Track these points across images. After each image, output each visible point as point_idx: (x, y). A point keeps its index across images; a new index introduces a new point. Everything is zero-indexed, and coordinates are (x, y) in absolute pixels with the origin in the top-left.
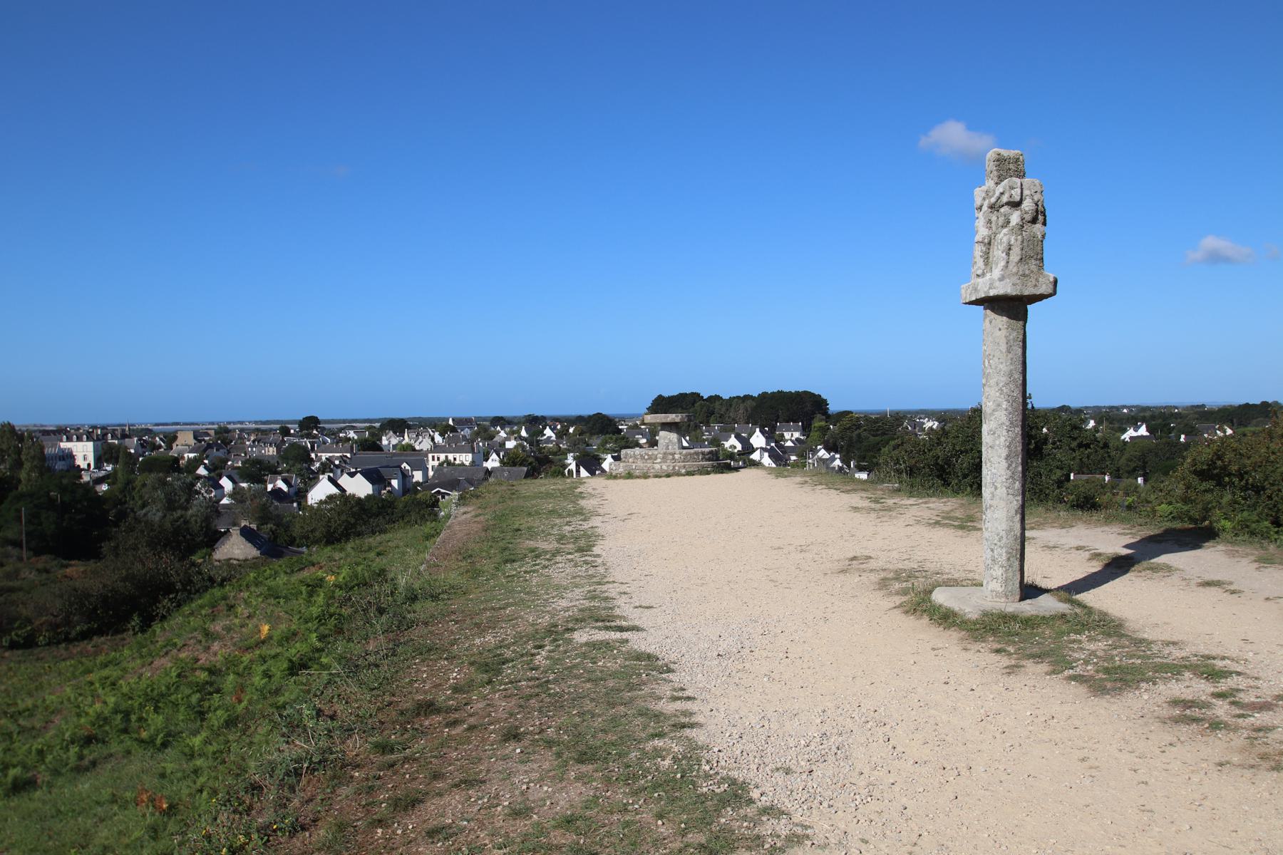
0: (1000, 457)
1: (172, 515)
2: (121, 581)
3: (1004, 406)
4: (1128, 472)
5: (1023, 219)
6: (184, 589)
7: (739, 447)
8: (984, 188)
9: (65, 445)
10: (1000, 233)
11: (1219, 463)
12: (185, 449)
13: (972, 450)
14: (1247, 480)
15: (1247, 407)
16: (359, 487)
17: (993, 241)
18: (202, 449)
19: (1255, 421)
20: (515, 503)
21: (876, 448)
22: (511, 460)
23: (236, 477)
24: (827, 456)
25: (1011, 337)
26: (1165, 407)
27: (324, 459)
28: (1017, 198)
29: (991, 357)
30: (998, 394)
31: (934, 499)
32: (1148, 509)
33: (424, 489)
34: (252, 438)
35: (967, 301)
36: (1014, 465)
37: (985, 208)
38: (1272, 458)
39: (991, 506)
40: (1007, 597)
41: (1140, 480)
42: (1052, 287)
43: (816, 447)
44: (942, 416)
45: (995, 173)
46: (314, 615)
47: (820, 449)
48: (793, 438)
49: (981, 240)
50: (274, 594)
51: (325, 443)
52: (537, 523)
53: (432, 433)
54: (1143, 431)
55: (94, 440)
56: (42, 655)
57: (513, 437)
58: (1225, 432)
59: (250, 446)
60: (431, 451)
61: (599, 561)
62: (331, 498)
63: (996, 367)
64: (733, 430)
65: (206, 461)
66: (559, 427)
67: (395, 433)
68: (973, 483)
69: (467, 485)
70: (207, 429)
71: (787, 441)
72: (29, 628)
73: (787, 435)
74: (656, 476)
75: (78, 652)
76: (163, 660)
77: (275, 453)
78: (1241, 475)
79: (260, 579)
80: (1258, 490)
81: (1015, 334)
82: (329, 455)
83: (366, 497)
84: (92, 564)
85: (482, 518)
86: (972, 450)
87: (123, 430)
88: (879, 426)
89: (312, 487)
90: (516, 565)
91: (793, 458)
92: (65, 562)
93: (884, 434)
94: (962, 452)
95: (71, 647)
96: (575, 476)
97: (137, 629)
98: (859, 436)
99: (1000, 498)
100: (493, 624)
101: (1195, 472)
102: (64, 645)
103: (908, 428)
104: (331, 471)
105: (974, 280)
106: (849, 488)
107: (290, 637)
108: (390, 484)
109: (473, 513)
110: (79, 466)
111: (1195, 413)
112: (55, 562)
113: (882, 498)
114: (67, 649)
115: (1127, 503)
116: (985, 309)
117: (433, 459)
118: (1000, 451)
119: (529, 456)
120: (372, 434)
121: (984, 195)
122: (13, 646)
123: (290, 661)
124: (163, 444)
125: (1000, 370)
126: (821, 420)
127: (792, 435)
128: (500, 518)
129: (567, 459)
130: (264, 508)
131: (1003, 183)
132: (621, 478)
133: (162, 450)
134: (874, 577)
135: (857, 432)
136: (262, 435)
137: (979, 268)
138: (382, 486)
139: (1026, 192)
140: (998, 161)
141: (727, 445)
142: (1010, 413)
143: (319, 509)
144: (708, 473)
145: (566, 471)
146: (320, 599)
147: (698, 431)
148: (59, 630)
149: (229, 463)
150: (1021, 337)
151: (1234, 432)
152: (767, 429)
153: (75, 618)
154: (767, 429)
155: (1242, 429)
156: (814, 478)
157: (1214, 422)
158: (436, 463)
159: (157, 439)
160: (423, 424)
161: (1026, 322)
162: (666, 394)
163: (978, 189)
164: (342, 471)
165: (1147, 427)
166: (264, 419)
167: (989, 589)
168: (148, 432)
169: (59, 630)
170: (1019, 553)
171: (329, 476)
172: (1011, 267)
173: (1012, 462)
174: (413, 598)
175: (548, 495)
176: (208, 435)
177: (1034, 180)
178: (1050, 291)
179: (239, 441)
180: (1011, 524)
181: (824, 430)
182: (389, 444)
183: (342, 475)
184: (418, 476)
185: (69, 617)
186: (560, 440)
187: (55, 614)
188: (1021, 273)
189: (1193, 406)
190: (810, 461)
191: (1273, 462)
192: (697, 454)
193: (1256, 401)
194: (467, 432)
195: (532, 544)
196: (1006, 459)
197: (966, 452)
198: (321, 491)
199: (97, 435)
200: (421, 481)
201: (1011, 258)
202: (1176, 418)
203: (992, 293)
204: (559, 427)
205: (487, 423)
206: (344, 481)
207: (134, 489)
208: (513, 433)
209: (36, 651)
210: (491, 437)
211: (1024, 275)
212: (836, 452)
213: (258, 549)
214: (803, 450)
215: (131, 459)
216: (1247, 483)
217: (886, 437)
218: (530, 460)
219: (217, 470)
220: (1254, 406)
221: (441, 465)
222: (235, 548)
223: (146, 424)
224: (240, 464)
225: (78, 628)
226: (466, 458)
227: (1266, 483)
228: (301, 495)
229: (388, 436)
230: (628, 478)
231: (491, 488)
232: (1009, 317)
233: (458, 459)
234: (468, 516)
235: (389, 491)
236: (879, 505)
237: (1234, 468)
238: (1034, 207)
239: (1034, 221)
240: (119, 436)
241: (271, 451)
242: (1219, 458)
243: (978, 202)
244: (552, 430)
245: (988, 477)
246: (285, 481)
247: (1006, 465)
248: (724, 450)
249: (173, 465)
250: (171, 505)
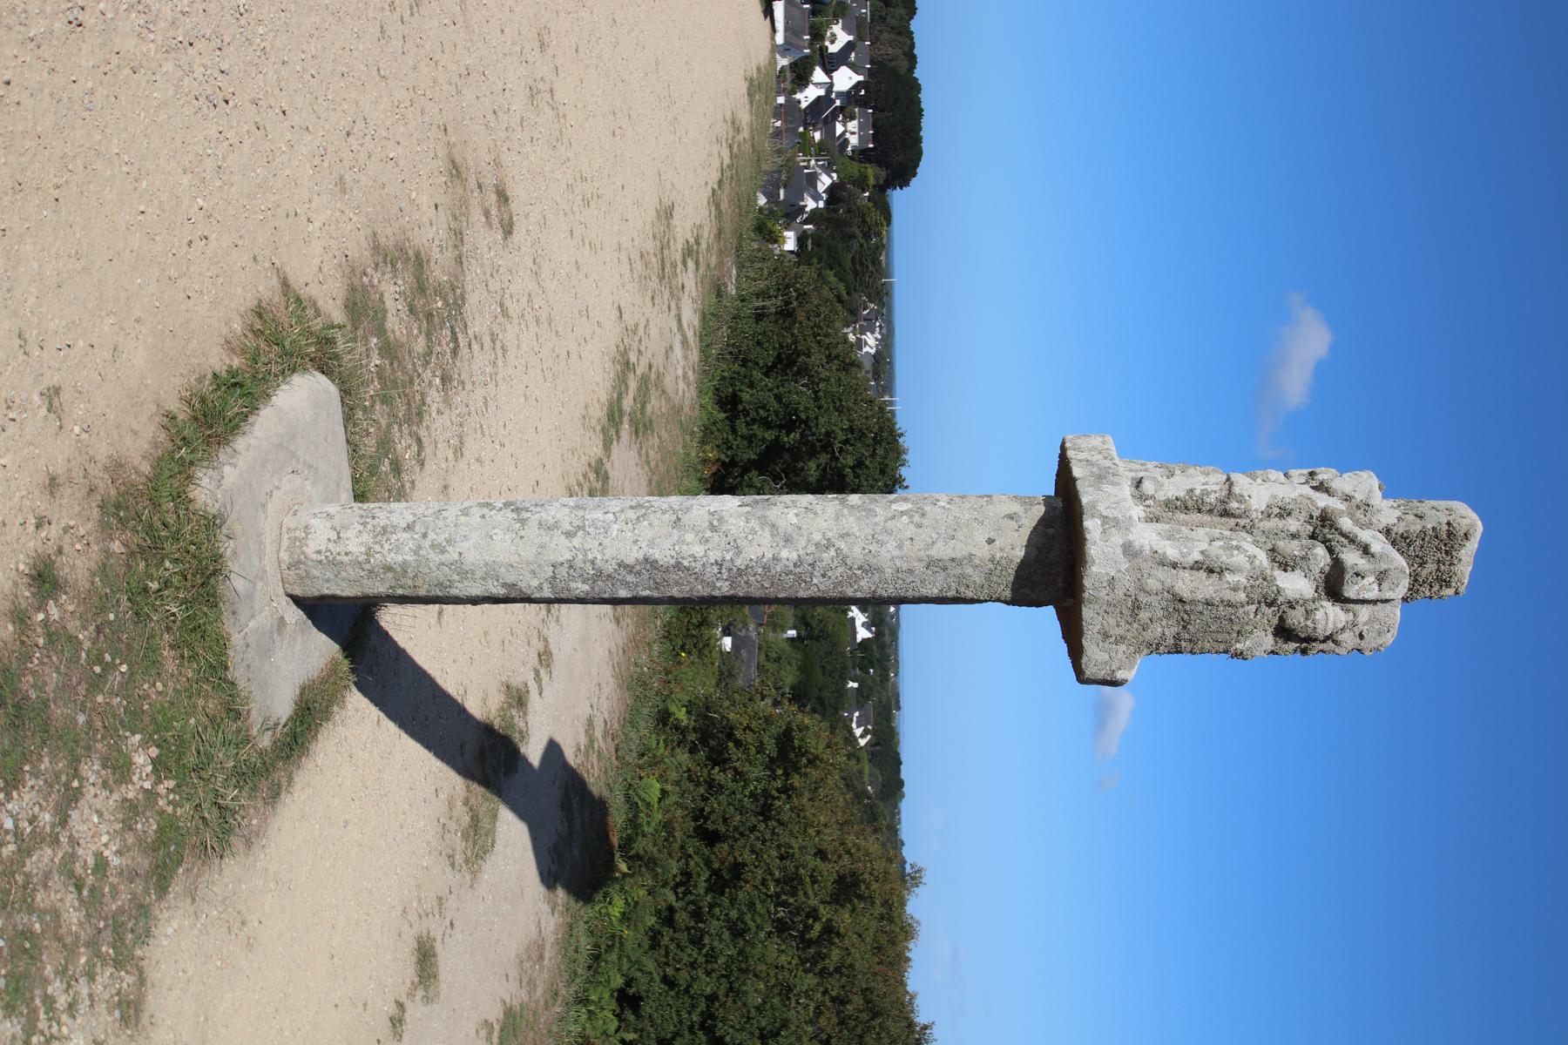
0: (652, 544)
3: (784, 554)
4: (803, 617)
5: (1291, 605)
7: (833, 48)
8: (1377, 499)
10: (1256, 543)
11: (804, 760)
13: (820, 407)
14: (778, 798)
15: (898, 762)
17: (1232, 521)
19: (878, 772)
21: (834, 263)
24: (821, 188)
25: (969, 571)
26: (897, 661)
28: (1350, 591)
29: (917, 518)
30: (817, 537)
31: (695, 356)
32: (661, 750)
35: (1070, 454)
36: (630, 578)
37: (1322, 501)
38: (811, 831)
39: (523, 522)
40: (295, 565)
41: (792, 633)
42: (1101, 675)
43: (835, 171)
44: (883, 360)
45: (1417, 527)
47: (831, 178)
48: (848, 135)
49: (1236, 490)
54: (863, 634)
58: (862, 736)
63: (889, 532)
64: (860, 38)
68: (769, 410)
71: (845, 125)
73: (853, 125)
78: (786, 790)
80: (765, 812)
81: (978, 578)
86: (820, 407)
88: (867, 267)
93: (856, 274)
94: (816, 392)
98: (853, 236)
99: (542, 546)
101: (788, 731)
103: (865, 309)
105: (1126, 471)
106: (724, 206)
111: (889, 700)
113: (697, 264)
115: (673, 708)
116: (1047, 500)
118: (667, 544)
121: (1359, 497)
125: (881, 543)
126: (876, 178)
127: (853, 133)
131: (1395, 554)
134: (430, 235)
135: (858, 233)
137: (1159, 486)
139: (1364, 612)
140: (1450, 534)
141: (837, 29)
142: (766, 568)
150: (969, 594)
151: (861, 748)
152: (863, 92)
154: (863, 92)
155: (865, 757)
156: (748, 145)
157: (875, 724)
161: (1007, 603)
163: (1375, 482)
165: (868, 639)
167: (313, 522)
170: (407, 592)
172: (1161, 573)
173: (639, 573)
177: (1394, 632)
178: (1089, 672)
180: (479, 574)
181: (861, 183)
188: (1143, 598)
189: (897, 695)
190: (813, 162)
191: (805, 832)
193: (905, 773)
196: (646, 560)
197: (817, 399)
201: (1186, 574)
202: (881, 675)
203: (1091, 525)
211: (1136, 607)
212: (827, 202)
214: (832, 151)
216: (774, 798)
217: (851, 277)
220: (898, 771)
227: (775, 824)
232: (1023, 565)
236: (678, 257)
237: (796, 781)
238: (1321, 632)
239: (1283, 632)
242: (811, 762)
243: (1344, 483)
245: (599, 515)
247: (630, 561)
248: (828, 25)
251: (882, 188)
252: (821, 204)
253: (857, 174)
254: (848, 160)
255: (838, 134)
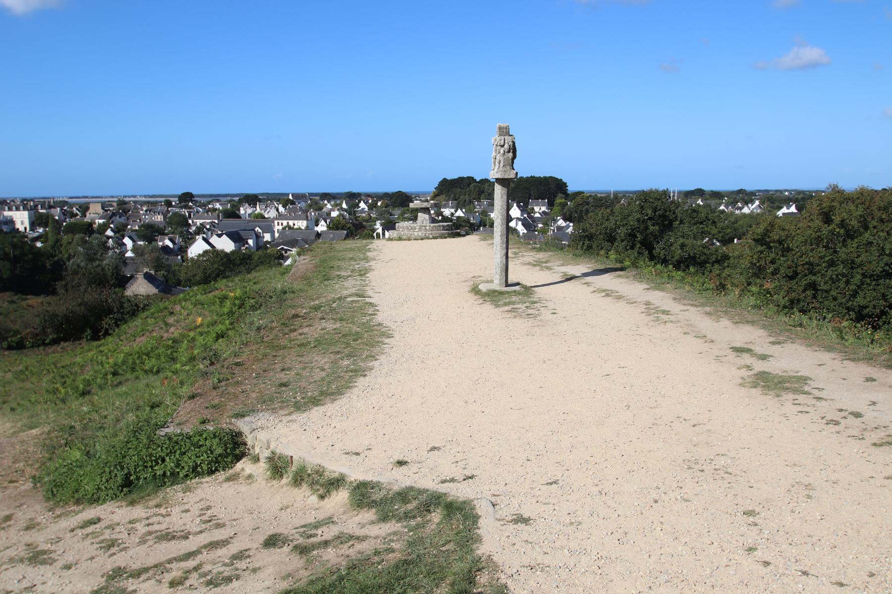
1: (92, 264)
2: (77, 306)
6: (118, 312)
9: (7, 213)
12: (95, 216)
13: (627, 224)
16: (225, 245)
18: (108, 216)
20: (332, 254)
22: (335, 226)
23: (135, 238)
27: (198, 224)
33: (272, 246)
34: (144, 209)
46: (226, 313)
47: (559, 219)
48: (541, 211)
50: (197, 304)
51: (198, 212)
52: (343, 264)
53: (277, 205)
54: (793, 209)
55: (28, 210)
56: (28, 354)
57: (336, 209)
59: (143, 214)
60: (277, 219)
61: (368, 279)
62: (206, 252)
65: (112, 226)
66: (370, 201)
67: (250, 205)
69: (303, 243)
70: (109, 201)
71: (536, 212)
72: (19, 336)
73: (536, 209)
74: (415, 239)
75: (52, 352)
76: (142, 338)
77: (162, 220)
79: (188, 297)
82: (202, 221)
83: (231, 252)
84: (49, 299)
85: (314, 261)
86: (627, 224)
87: (49, 202)
89: (191, 244)
90: (330, 281)
91: (540, 225)
92: (24, 297)
95: (47, 349)
96: (381, 237)
97: (89, 338)
100: (318, 298)
101: (754, 240)
102: (42, 347)
104: (204, 233)
107: (214, 324)
108: (247, 243)
109: (309, 259)
110: (18, 229)
112: (17, 297)
114: (44, 350)
117: (278, 225)
119: (349, 223)
120: (232, 206)
122: (10, 348)
123: (217, 333)
124: (78, 213)
126: (562, 198)
128: (324, 261)
129: (375, 225)
130: (158, 259)
132: (395, 240)
133: (78, 217)
136: (152, 206)
138: (242, 244)
139: (506, 142)
143: (198, 260)
144: (446, 238)
145: (375, 234)
146: (228, 303)
147: (472, 205)
148: (39, 338)
149: (129, 227)
152: (522, 204)
153: (49, 330)
154: (522, 204)
158: (280, 227)
159: (74, 209)
160: (270, 198)
162: (449, 178)
164: (212, 233)
165: (796, 206)
166: (151, 194)
168: (65, 203)
169: (39, 338)
171: (203, 237)
174: (285, 292)
175: (351, 250)
176: (112, 206)
179: (135, 211)
182: (246, 213)
183: (212, 236)
184: (267, 237)
185: (44, 330)
186: (371, 211)
187: (35, 327)
190: (552, 228)
192: (439, 226)
194: (303, 204)
195: (338, 273)
197: (623, 226)
198: (197, 248)
199: (31, 206)
200: (270, 240)
204: (370, 201)
205: (318, 198)
206: (214, 240)
207: (61, 246)
208: (336, 205)
209: (25, 351)
210: (321, 209)
212: (570, 222)
213: (157, 288)
214: (548, 219)
215: (58, 223)
218: (349, 226)
219: (120, 231)
221: (284, 229)
222: (140, 288)
223: (63, 197)
224: (137, 228)
225: (51, 336)
226: (302, 224)
228: (183, 250)
229: (245, 207)
230: (399, 240)
231: (319, 246)
233: (296, 225)
234: (306, 261)
235: (247, 248)
238: (508, 147)
240: (47, 207)
241: (159, 218)
244: (365, 203)
246: (171, 240)
249: (89, 228)
250: (91, 259)
251: (566, 195)
252: (571, 224)
253: (559, 207)
254: (552, 212)
255: (539, 216)
